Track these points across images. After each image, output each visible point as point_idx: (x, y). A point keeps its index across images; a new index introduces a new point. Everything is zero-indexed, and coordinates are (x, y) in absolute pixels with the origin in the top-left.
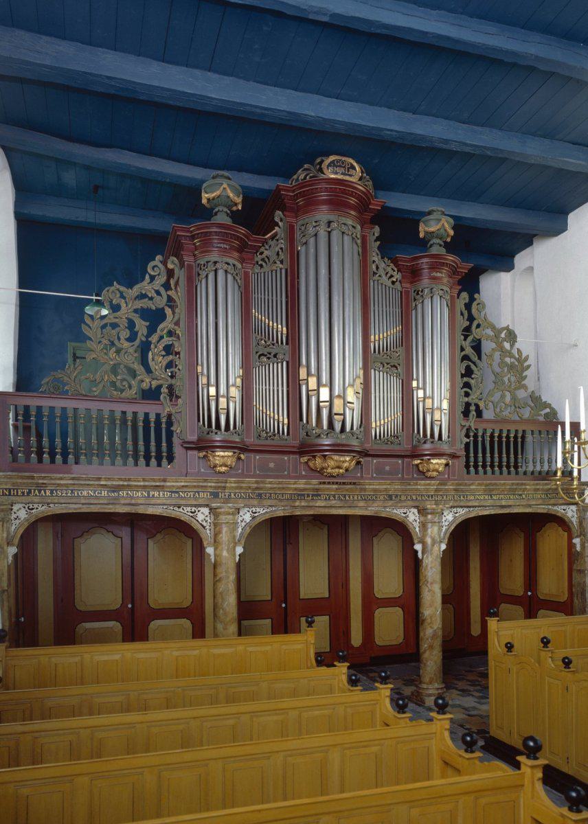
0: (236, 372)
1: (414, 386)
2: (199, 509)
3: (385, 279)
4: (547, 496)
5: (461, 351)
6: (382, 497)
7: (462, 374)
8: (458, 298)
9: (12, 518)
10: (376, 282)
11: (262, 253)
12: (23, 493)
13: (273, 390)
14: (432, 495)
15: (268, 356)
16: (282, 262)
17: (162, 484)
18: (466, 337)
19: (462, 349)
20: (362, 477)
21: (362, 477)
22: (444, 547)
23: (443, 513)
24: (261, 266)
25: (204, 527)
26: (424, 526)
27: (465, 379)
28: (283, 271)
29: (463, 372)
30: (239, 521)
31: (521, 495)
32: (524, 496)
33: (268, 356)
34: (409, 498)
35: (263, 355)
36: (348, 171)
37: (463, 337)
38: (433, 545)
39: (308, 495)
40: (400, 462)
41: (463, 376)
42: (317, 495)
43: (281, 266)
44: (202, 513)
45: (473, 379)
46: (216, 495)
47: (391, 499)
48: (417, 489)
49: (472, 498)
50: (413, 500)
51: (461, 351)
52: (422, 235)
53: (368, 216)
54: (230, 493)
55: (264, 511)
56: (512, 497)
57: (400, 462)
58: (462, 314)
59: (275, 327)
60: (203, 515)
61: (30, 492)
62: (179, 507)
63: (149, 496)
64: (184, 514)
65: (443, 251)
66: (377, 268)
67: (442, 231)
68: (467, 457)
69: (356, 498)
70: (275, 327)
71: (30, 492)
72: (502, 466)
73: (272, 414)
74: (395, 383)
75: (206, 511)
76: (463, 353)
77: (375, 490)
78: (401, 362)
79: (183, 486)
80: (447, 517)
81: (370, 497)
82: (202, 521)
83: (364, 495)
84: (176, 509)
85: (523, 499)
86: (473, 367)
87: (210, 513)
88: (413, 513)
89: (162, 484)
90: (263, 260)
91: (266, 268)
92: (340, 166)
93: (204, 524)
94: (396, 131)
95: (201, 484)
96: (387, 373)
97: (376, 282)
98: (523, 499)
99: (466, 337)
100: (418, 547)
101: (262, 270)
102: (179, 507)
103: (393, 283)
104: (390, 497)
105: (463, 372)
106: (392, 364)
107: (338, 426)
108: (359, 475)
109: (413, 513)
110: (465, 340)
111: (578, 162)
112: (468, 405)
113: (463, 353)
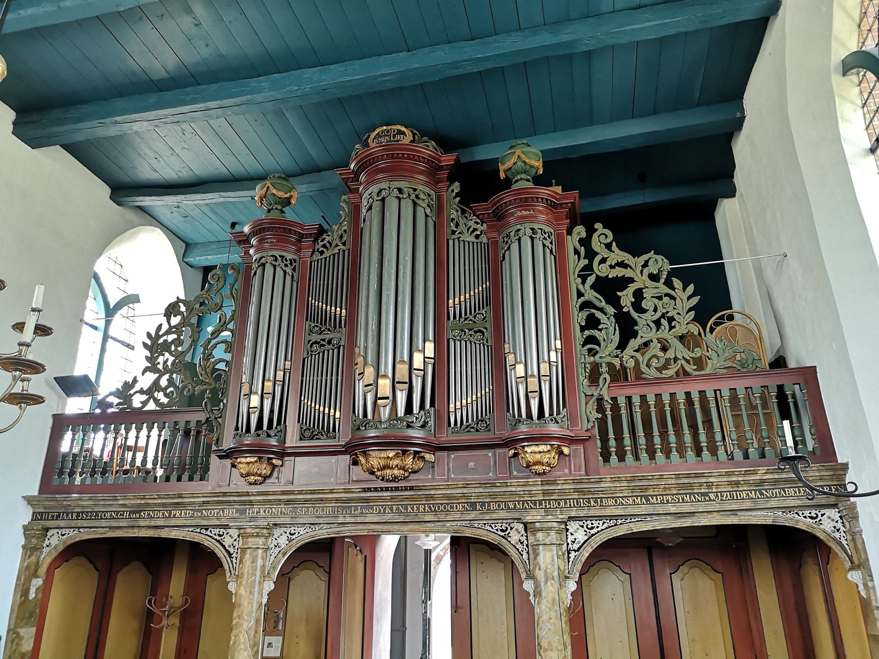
1: (432, 345)
2: (823, 512)
3: (469, 238)
4: (762, 494)
5: (579, 297)
6: (460, 507)
7: (581, 326)
8: (568, 234)
9: (45, 545)
10: (456, 241)
11: (324, 239)
12: (53, 517)
13: (332, 380)
14: (540, 501)
15: (322, 342)
16: (344, 244)
17: (180, 500)
18: (584, 279)
19: (580, 294)
20: (433, 479)
21: (433, 479)
23: (567, 530)
24: (322, 253)
25: (230, 555)
27: (587, 333)
28: (346, 252)
29: (583, 324)
30: (272, 546)
31: (703, 494)
32: (712, 496)
33: (322, 342)
34: (503, 506)
35: (316, 343)
36: (394, 137)
37: (579, 280)
39: (356, 508)
40: (490, 454)
41: (583, 329)
42: (367, 508)
43: (344, 248)
44: (829, 518)
45: (600, 330)
47: (475, 509)
48: (512, 493)
49: (611, 502)
50: (509, 508)
51: (579, 297)
52: (502, 176)
53: (444, 174)
54: (59, 513)
55: (606, 525)
56: (687, 499)
57: (490, 454)
58: (577, 252)
59: (338, 313)
61: (58, 516)
62: (207, 529)
63: (170, 517)
65: (530, 185)
66: (457, 225)
67: (519, 163)
68: (605, 440)
69: (421, 509)
70: (338, 313)
71: (58, 516)
72: (625, 451)
73: (322, 408)
74: (483, 356)
76: (582, 299)
77: (448, 497)
78: (488, 325)
79: (204, 502)
80: (576, 535)
81: (442, 508)
82: (230, 546)
83: (433, 504)
84: (203, 531)
85: (710, 500)
86: (598, 314)
87: (239, 536)
88: (517, 530)
89: (180, 500)
90: (324, 246)
91: (327, 254)
92: (385, 135)
93: (231, 550)
94: (390, 74)
95: (221, 499)
96: (471, 342)
97: (456, 241)
98: (710, 500)
99: (584, 279)
100: (528, 586)
101: (324, 256)
102: (207, 529)
103: (477, 237)
104: (473, 506)
105: (583, 324)
106: (476, 329)
108: (430, 476)
109: (517, 530)
110: (583, 283)
111: (650, 24)
112: (596, 367)
113: (582, 299)
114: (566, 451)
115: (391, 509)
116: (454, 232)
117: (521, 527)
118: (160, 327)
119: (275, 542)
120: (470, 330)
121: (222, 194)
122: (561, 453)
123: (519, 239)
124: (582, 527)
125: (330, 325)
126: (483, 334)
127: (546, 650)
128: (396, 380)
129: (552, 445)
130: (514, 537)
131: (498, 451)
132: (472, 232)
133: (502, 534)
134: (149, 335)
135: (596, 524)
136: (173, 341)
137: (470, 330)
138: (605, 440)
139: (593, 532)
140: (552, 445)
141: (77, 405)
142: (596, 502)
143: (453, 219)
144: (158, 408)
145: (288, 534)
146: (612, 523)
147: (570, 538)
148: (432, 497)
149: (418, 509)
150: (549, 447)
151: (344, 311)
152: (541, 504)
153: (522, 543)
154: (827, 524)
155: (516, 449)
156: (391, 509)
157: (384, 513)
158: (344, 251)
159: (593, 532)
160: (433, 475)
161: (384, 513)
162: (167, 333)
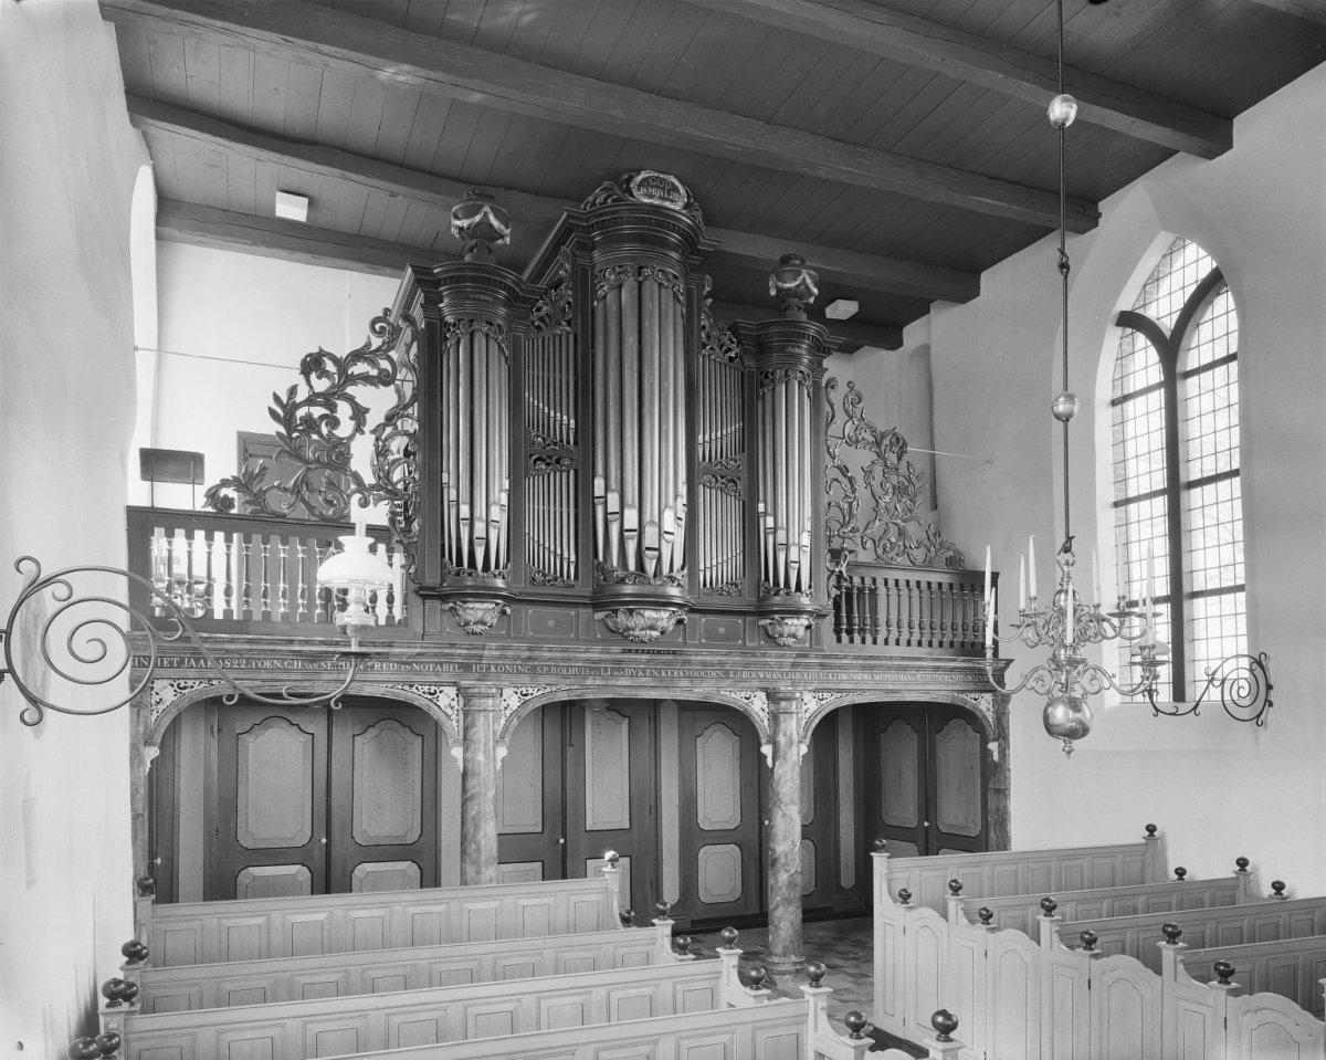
0: (501, 483)
11: (539, 310)
12: (171, 663)
22: (804, 749)
26: (775, 718)
28: (571, 337)
38: (775, 718)
39: (606, 669)
42: (616, 669)
46: (466, 668)
60: (447, 698)
62: (411, 686)
64: (417, 696)
74: (733, 507)
75: (452, 691)
79: (418, 654)
81: (696, 674)
93: (449, 711)
102: (411, 686)
107: (650, 567)
114: (509, 611)
115: (644, 672)
116: (704, 346)
117: (763, 695)
118: (293, 391)
119: (504, 704)
120: (722, 477)
121: (347, 174)
122: (503, 613)
123: (472, 335)
124: (172, 686)
125: (543, 432)
126: (736, 486)
127: (786, 804)
128: (461, 516)
129: (497, 604)
130: (443, 701)
131: (748, 619)
132: (726, 352)
133: (430, 697)
134: (277, 398)
135: (825, 695)
136: (322, 417)
137: (722, 477)
138: (837, 616)
139: (527, 698)
140: (497, 604)
141: (178, 496)
142: (496, 668)
143: (704, 327)
144: (210, 509)
145: (175, 687)
146: (839, 695)
147: (804, 707)
148: (689, 662)
149: (672, 673)
150: (493, 605)
151: (572, 421)
152: (787, 675)
153: (452, 708)
154: (985, 704)
155: (455, 603)
156: (644, 672)
157: (637, 676)
158: (568, 333)
159: (527, 698)
160: (684, 639)
161: (637, 676)
162: (310, 401)
